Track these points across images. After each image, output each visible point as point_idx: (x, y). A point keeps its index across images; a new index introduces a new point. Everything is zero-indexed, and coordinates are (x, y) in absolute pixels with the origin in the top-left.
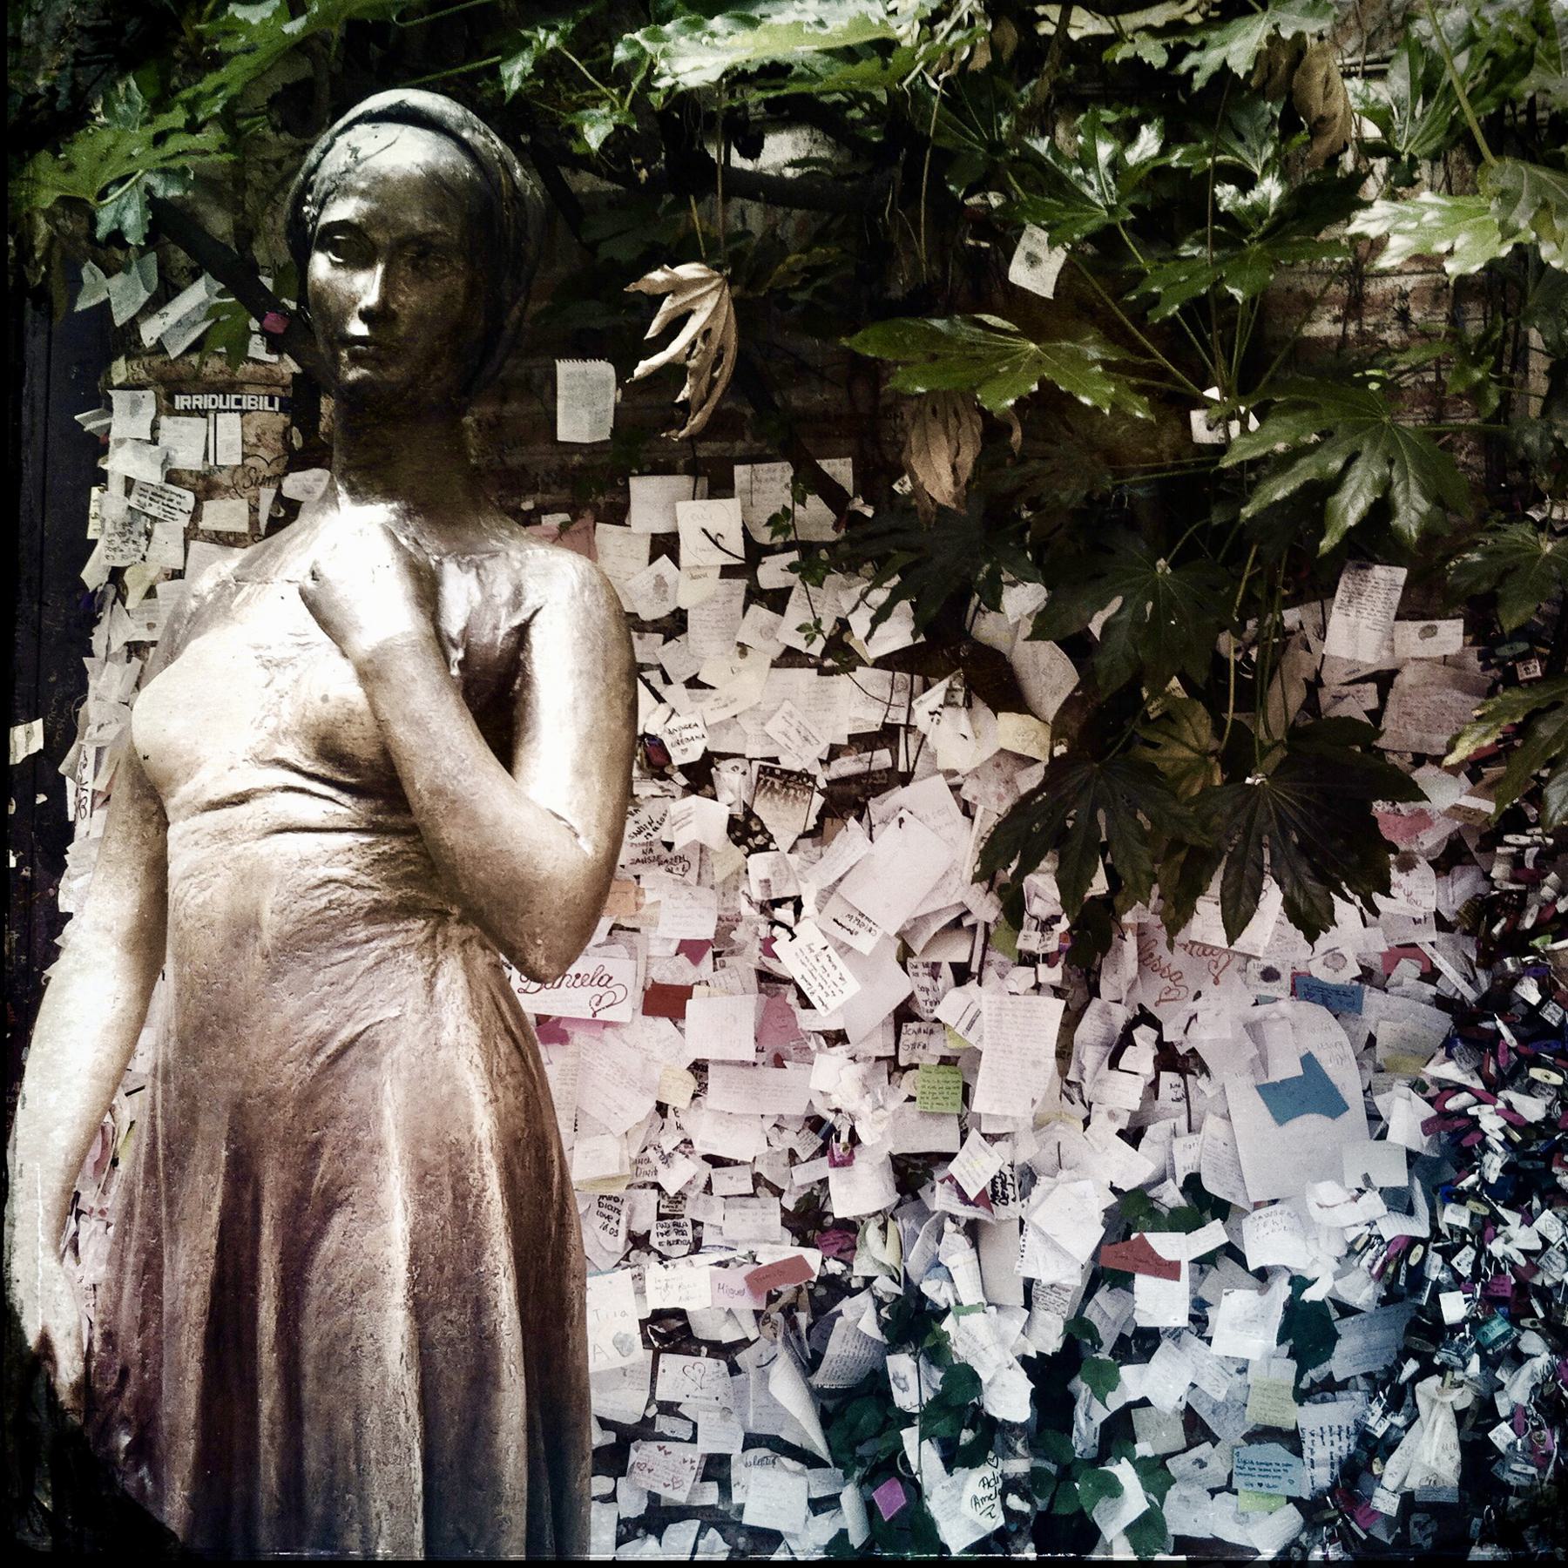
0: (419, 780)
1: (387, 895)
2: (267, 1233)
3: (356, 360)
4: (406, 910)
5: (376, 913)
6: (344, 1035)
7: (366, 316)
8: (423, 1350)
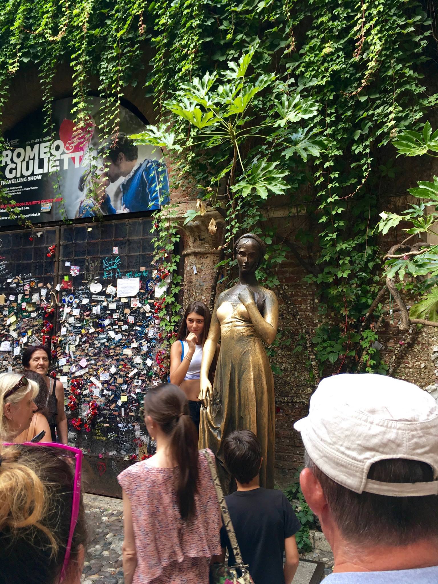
0: (253, 320)
1: (250, 334)
2: (236, 374)
3: (244, 268)
4: (251, 336)
5: (249, 336)
7: (245, 263)
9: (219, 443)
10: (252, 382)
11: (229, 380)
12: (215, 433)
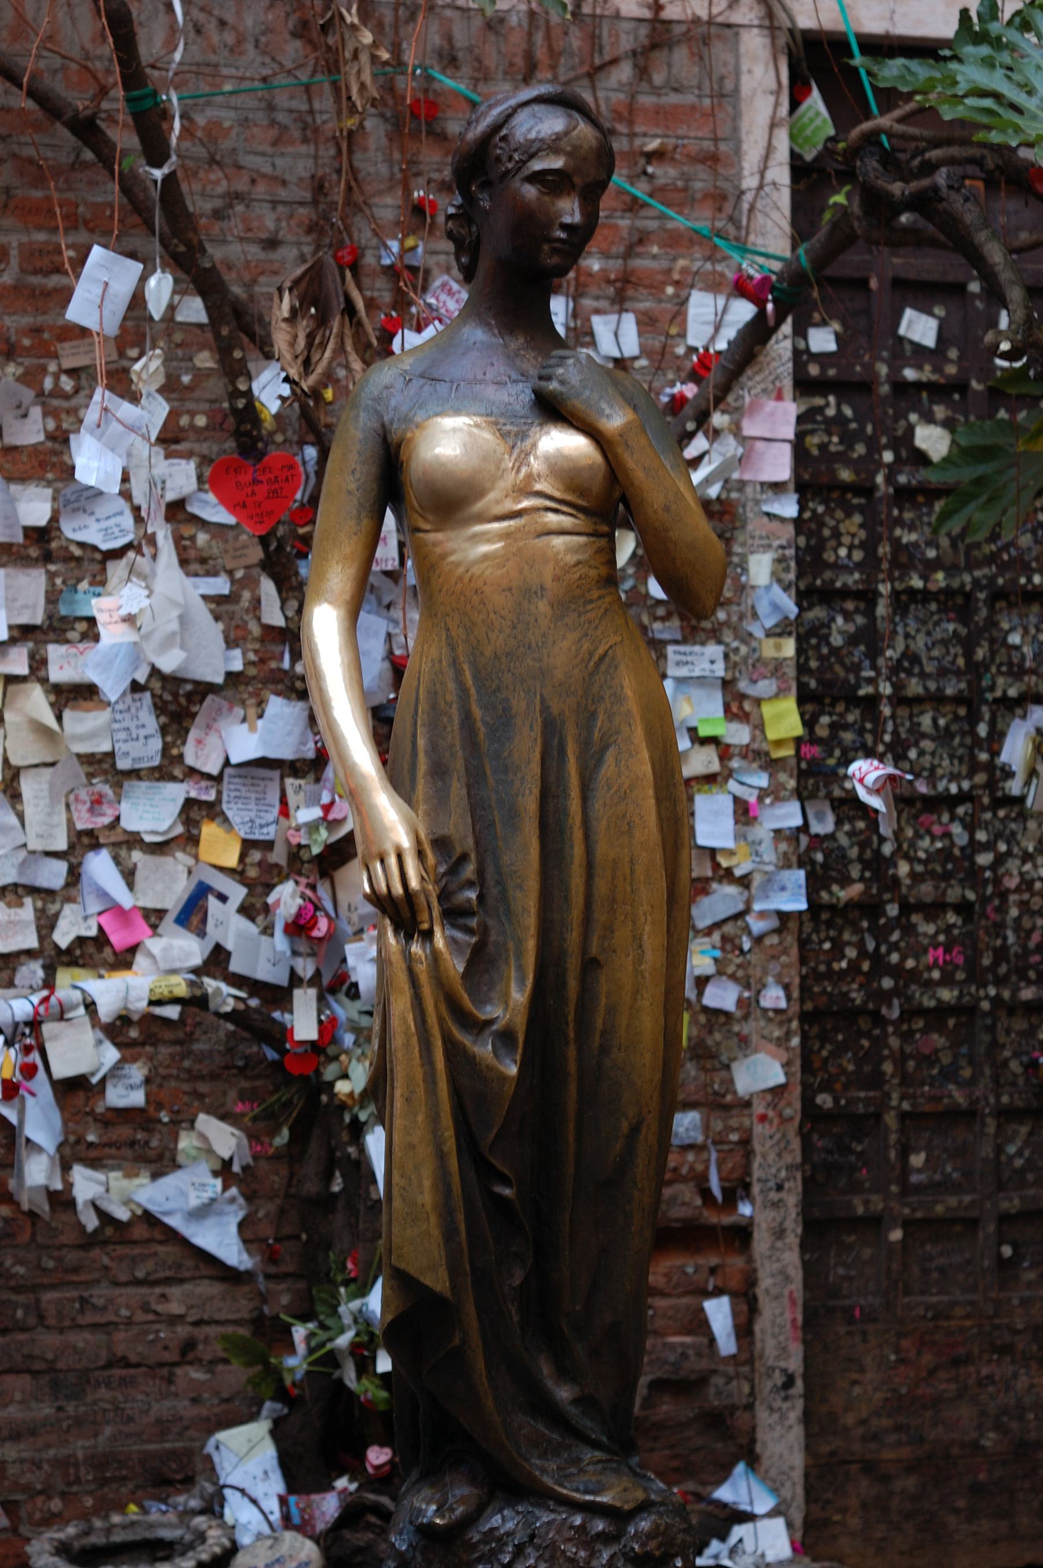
3: (555, 251)
6: (601, 651)
8: (660, 819)
9: (509, 1089)
10: (651, 792)
11: (536, 791)
12: (484, 1050)
